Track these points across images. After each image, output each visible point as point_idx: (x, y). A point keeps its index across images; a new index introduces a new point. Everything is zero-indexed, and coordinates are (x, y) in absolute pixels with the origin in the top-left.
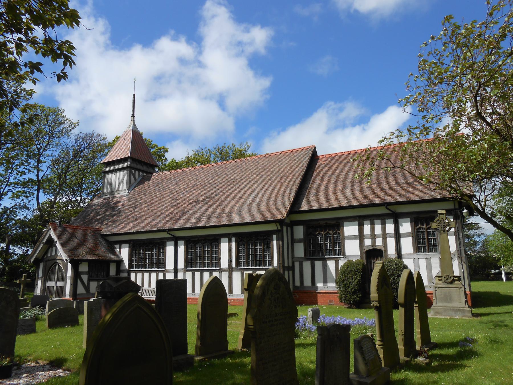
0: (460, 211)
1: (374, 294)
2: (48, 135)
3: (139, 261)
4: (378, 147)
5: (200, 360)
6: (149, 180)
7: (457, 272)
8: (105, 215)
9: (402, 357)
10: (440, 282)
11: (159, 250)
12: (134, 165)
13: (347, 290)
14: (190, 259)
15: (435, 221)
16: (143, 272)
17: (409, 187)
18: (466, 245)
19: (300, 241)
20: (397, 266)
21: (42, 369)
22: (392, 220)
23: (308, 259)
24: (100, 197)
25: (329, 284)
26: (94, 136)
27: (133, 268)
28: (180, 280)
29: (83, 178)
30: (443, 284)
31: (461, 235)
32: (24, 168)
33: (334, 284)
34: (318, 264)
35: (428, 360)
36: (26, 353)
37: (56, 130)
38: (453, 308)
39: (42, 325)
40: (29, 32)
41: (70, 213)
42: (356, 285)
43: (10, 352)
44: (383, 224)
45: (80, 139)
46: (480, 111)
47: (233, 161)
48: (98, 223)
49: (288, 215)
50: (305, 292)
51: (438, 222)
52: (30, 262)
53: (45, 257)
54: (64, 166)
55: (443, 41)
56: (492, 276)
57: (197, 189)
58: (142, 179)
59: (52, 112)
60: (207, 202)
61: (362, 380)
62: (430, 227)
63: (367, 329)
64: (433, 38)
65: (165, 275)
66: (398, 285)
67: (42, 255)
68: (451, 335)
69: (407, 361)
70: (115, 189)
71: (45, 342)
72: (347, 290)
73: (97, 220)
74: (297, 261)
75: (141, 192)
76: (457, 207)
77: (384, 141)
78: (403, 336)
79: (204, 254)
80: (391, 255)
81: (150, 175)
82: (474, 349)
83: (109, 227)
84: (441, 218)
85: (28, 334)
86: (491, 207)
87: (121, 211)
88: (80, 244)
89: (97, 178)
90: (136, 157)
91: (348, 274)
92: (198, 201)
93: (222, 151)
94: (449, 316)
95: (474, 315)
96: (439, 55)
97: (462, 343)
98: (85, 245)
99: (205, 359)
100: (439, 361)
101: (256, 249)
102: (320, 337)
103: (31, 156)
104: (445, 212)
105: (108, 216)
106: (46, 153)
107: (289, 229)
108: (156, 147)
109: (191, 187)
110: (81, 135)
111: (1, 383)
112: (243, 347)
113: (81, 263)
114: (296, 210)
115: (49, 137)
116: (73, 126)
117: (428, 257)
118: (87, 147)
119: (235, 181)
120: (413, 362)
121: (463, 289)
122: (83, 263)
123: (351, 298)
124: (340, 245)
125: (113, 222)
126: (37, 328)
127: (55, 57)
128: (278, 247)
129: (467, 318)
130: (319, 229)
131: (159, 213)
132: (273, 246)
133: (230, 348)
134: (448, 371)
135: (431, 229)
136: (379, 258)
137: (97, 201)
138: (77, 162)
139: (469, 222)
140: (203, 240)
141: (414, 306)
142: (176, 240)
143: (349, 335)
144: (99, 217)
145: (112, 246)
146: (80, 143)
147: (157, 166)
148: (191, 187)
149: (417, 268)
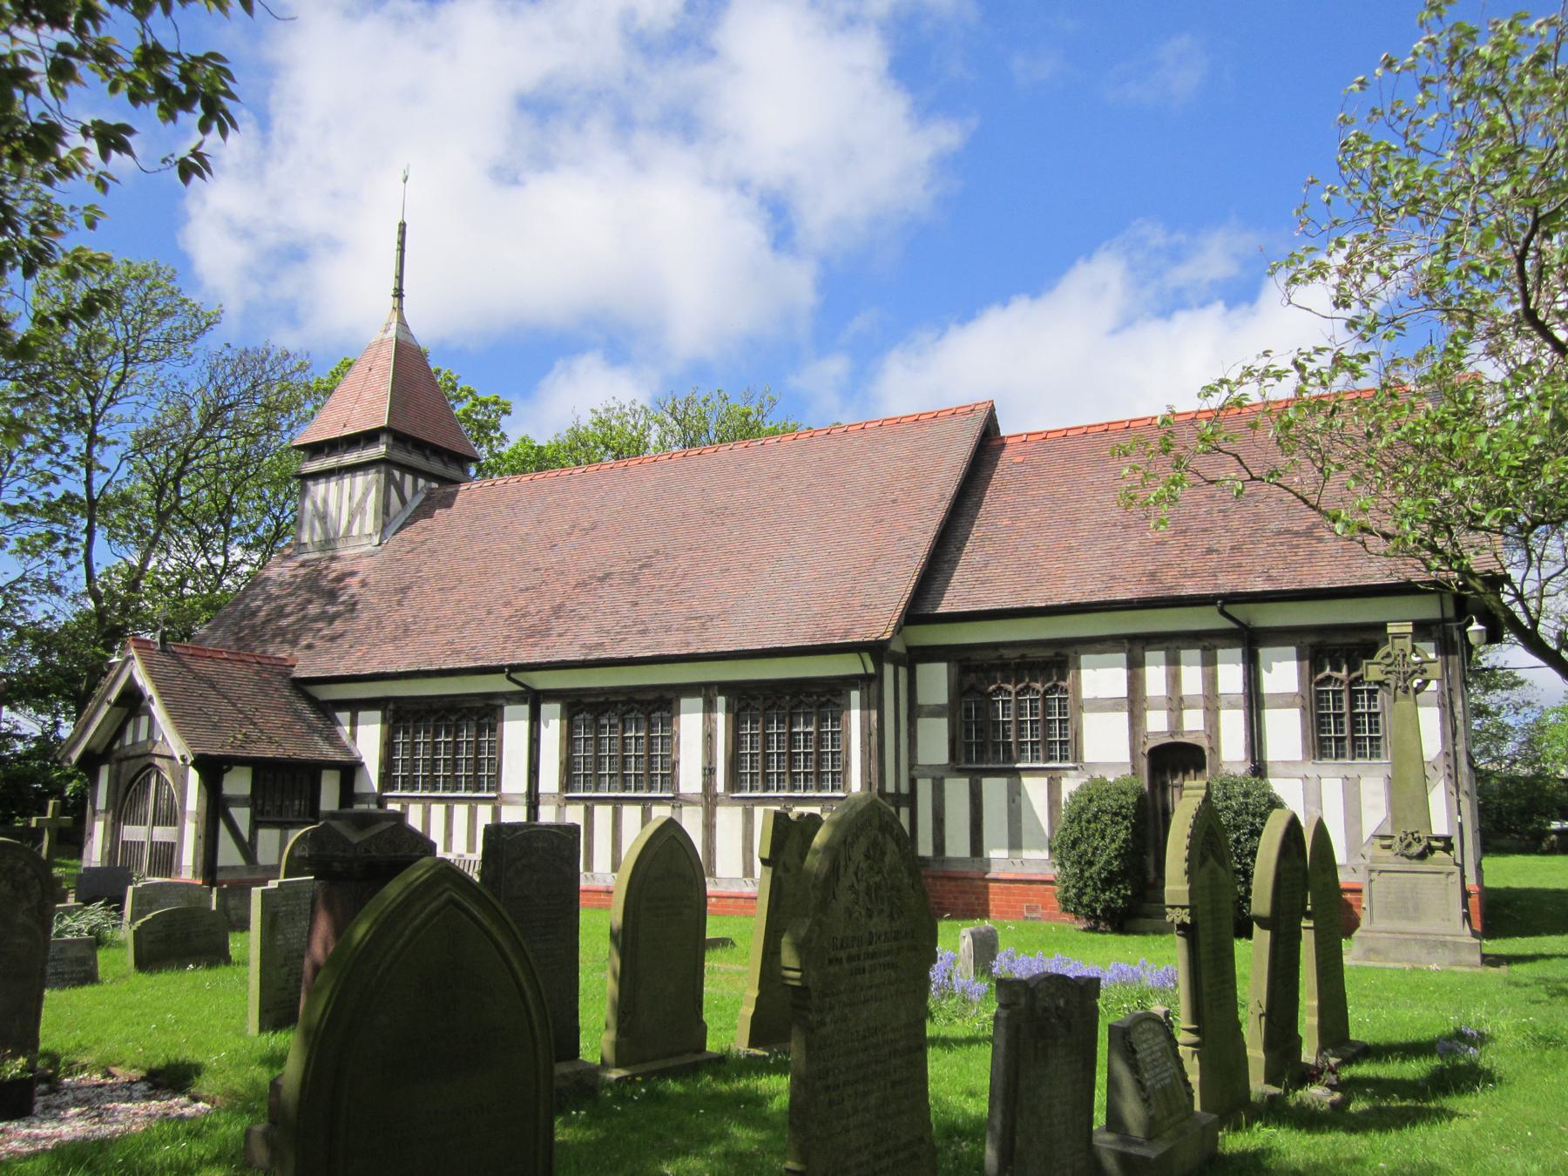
0: (1459, 628)
1: (1176, 884)
2: (121, 354)
3: (415, 767)
4: (1199, 412)
5: (619, 1080)
6: (449, 506)
7: (1440, 825)
8: (304, 617)
9: (1258, 1086)
10: (1388, 853)
11: (480, 732)
12: (401, 456)
13: (1087, 874)
14: (579, 763)
15: (1378, 658)
16: (428, 801)
17: (1298, 546)
18: (1473, 739)
19: (935, 712)
20: (1250, 801)
21: (125, 1093)
22: (1237, 652)
23: (961, 772)
24: (289, 557)
25: (1026, 854)
26: (270, 359)
27: (394, 788)
28: (548, 826)
29: (232, 493)
30: (1394, 859)
31: (1459, 704)
32: (51, 462)
33: (1045, 855)
34: (994, 789)
35: (1337, 1095)
36: (72, 1043)
37: (148, 337)
38: (1423, 937)
39: (117, 960)
40: (89, 23)
41: (191, 607)
42: (1116, 857)
43: (27, 1040)
44: (1209, 662)
45: (224, 368)
46: (1536, 304)
47: (724, 449)
48: (282, 642)
49: (898, 629)
50: (951, 878)
51: (1389, 661)
52: (70, 761)
53: (116, 746)
54: (173, 454)
55: (1421, 75)
56: (1554, 837)
57: (606, 538)
58: (424, 500)
59: (135, 278)
60: (635, 579)
61: (1134, 1150)
62: (1361, 677)
63: (1147, 997)
64: (1389, 64)
65: (496, 813)
66: (1253, 861)
67: (107, 741)
68: (1412, 1020)
69: (1272, 1098)
70: (337, 533)
71: (128, 1012)
72: (1087, 874)
73: (282, 632)
74: (924, 777)
75: (423, 543)
76: (1450, 612)
77: (1216, 391)
78: (1263, 1019)
79: (624, 747)
80: (1232, 763)
81: (450, 489)
82: (1484, 1063)
83: (319, 654)
84: (1397, 647)
85: (73, 986)
86: (1557, 615)
87: (355, 604)
88: (225, 706)
89: (276, 495)
90: (406, 428)
91: (1089, 822)
92: (608, 576)
93: (686, 413)
94: (1408, 961)
95: (1491, 960)
96: (1406, 119)
97: (1448, 1045)
98: (241, 712)
99: (633, 1076)
100: (1371, 1097)
101: (792, 735)
102: (1004, 1014)
103: (69, 421)
104: (1410, 629)
105: (316, 619)
106: (114, 411)
107: (903, 671)
108: (470, 397)
109: (586, 531)
110: (227, 353)
111: (2, 1132)
112: (753, 1042)
113: (229, 769)
114: (928, 610)
115: (126, 357)
116: (203, 324)
117: (1352, 773)
118: (246, 392)
119: (727, 512)
120: (1292, 1101)
121: (1457, 877)
122: (236, 768)
123: (1096, 900)
124: (1066, 729)
125: (333, 639)
126: (100, 969)
127: (173, 101)
128: (867, 731)
129: (1467, 970)
130: (998, 675)
131: (482, 613)
132: (848, 728)
133: (712, 1046)
134: (1399, 1128)
135: (1364, 683)
136: (1192, 772)
137: (280, 571)
138: (215, 442)
139: (1485, 665)
140: (623, 703)
141: (1300, 928)
142: (534, 700)
143: (1095, 1011)
144: (284, 622)
145: (326, 716)
146: (225, 380)
147: (476, 460)
148: (586, 531)
149: (1313, 809)
